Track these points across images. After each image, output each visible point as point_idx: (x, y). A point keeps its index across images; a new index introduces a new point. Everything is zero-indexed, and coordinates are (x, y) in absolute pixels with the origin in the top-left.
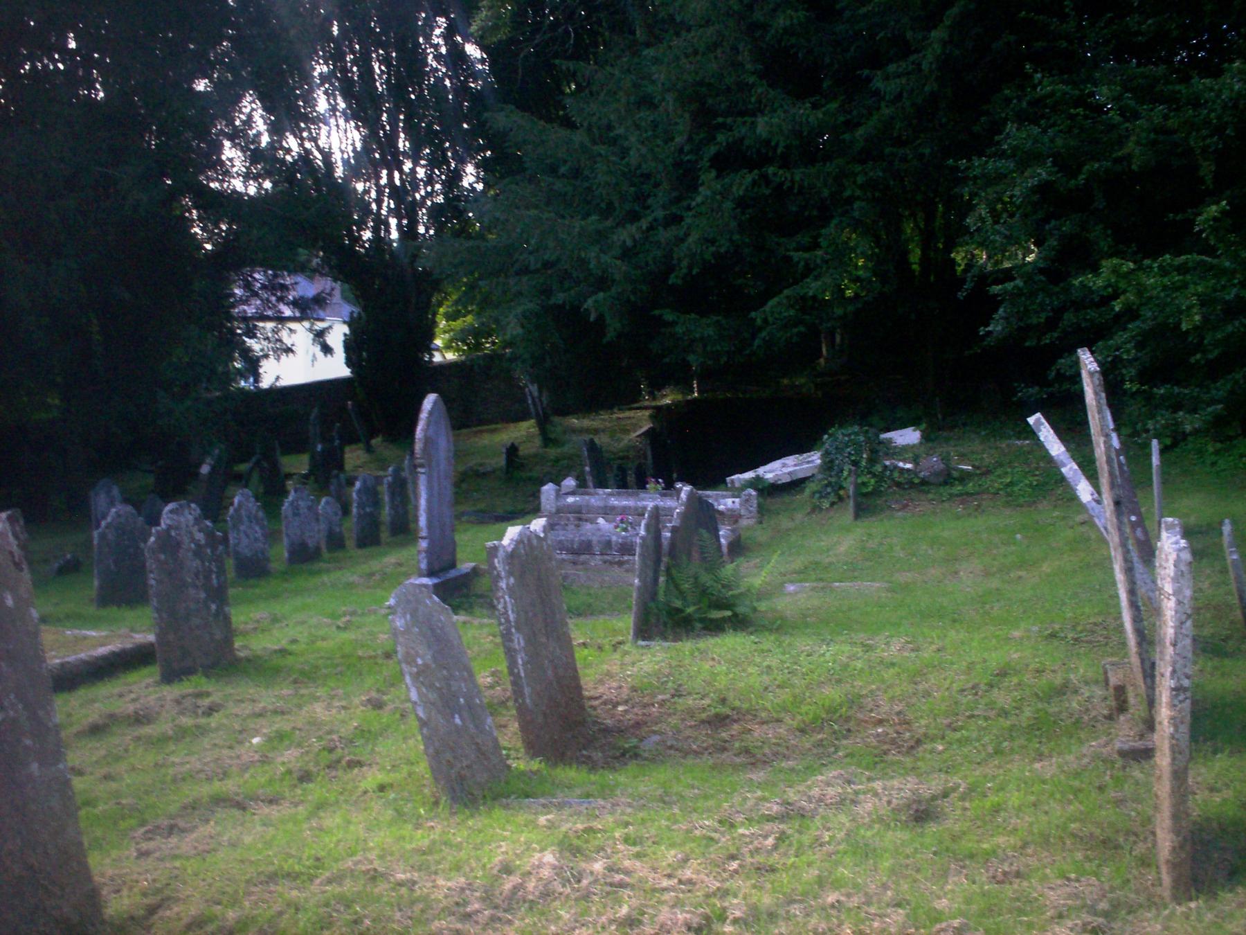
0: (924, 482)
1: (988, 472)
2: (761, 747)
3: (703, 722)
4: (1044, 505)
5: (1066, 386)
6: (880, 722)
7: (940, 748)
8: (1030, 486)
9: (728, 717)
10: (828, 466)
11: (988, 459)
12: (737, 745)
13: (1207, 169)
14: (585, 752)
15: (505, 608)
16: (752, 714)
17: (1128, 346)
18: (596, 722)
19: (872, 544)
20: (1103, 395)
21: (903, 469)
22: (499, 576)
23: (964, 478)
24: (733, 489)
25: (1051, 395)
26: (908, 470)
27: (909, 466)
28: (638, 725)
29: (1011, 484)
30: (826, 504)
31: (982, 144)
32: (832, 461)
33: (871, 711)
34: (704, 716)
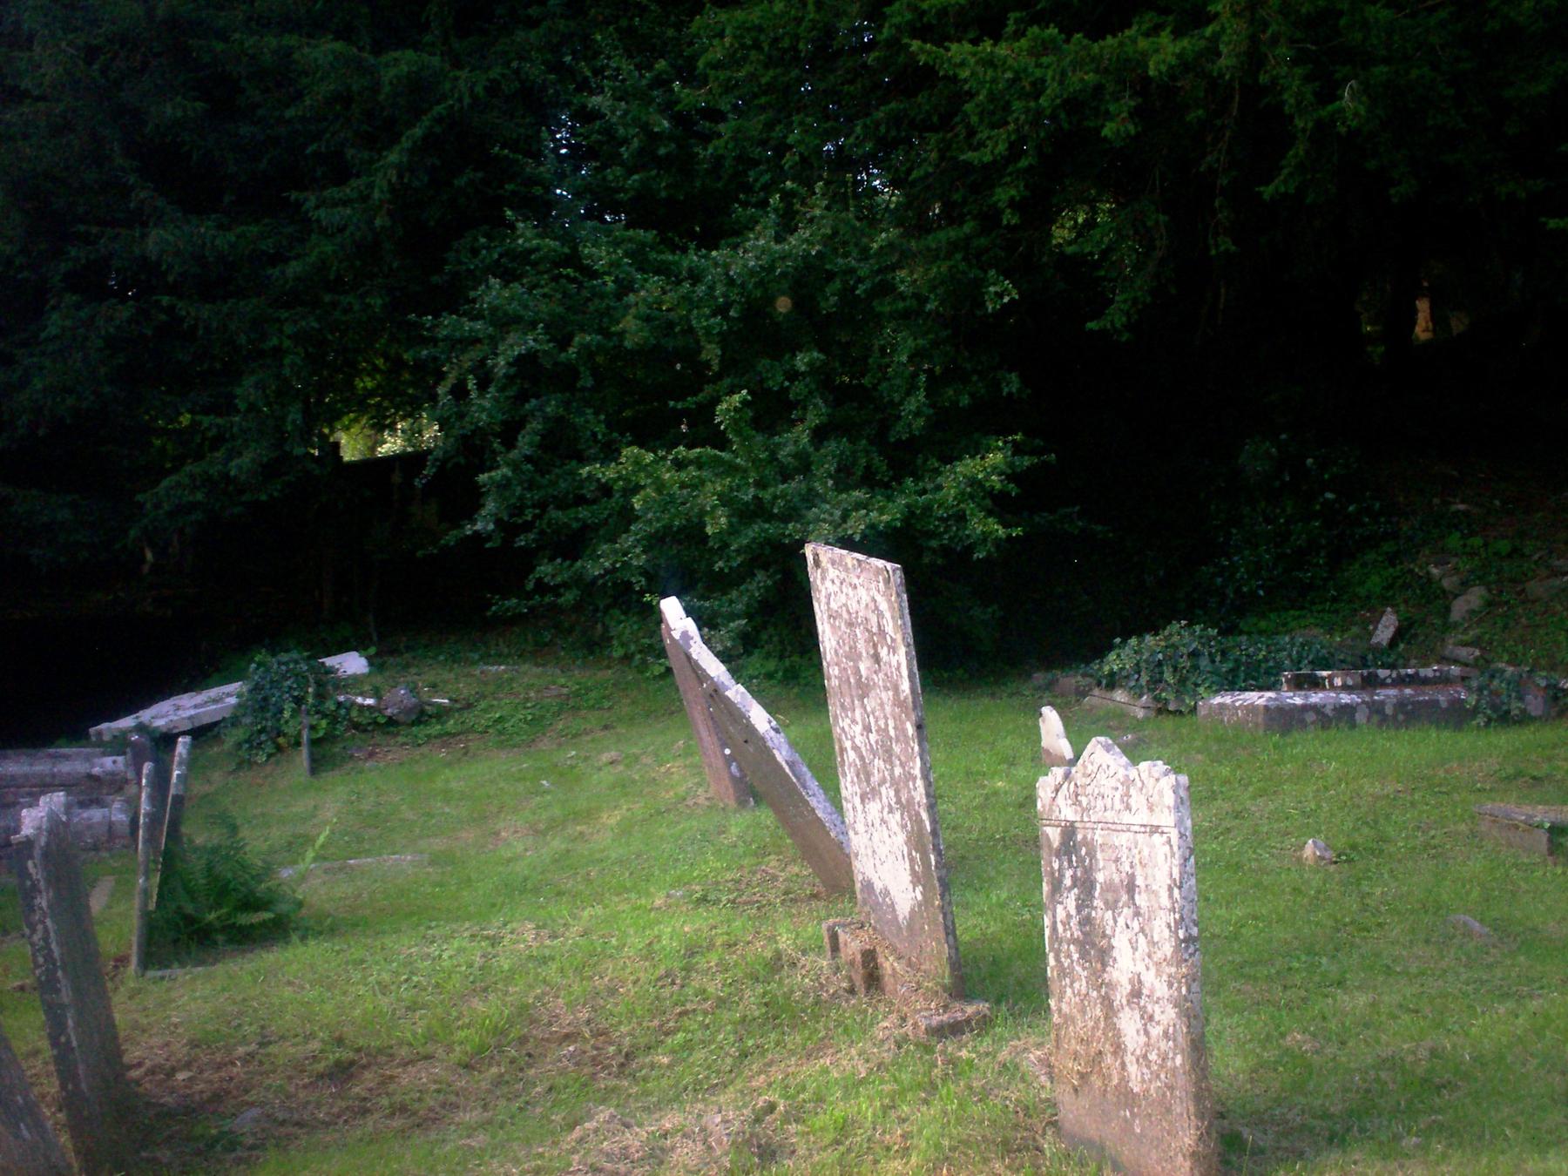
0: (391, 721)
1: (469, 706)
2: (420, 1100)
3: (321, 1076)
4: (545, 745)
5: (548, 599)
6: (567, 1037)
7: (666, 1060)
8: (526, 722)
9: (352, 1063)
10: (260, 704)
11: (465, 689)
12: (385, 1102)
13: (711, 353)
14: (144, 1154)
15: (46, 939)
16: (387, 1052)
17: (637, 551)
18: (148, 1103)
19: (366, 805)
20: (905, 596)
21: (362, 706)
22: (35, 888)
23: (441, 714)
24: (100, 743)
25: (532, 609)
26: (369, 706)
27: (370, 701)
28: (217, 1097)
29: (501, 720)
30: (262, 758)
31: (453, 298)
32: (265, 699)
33: (550, 1024)
34: (320, 1067)
